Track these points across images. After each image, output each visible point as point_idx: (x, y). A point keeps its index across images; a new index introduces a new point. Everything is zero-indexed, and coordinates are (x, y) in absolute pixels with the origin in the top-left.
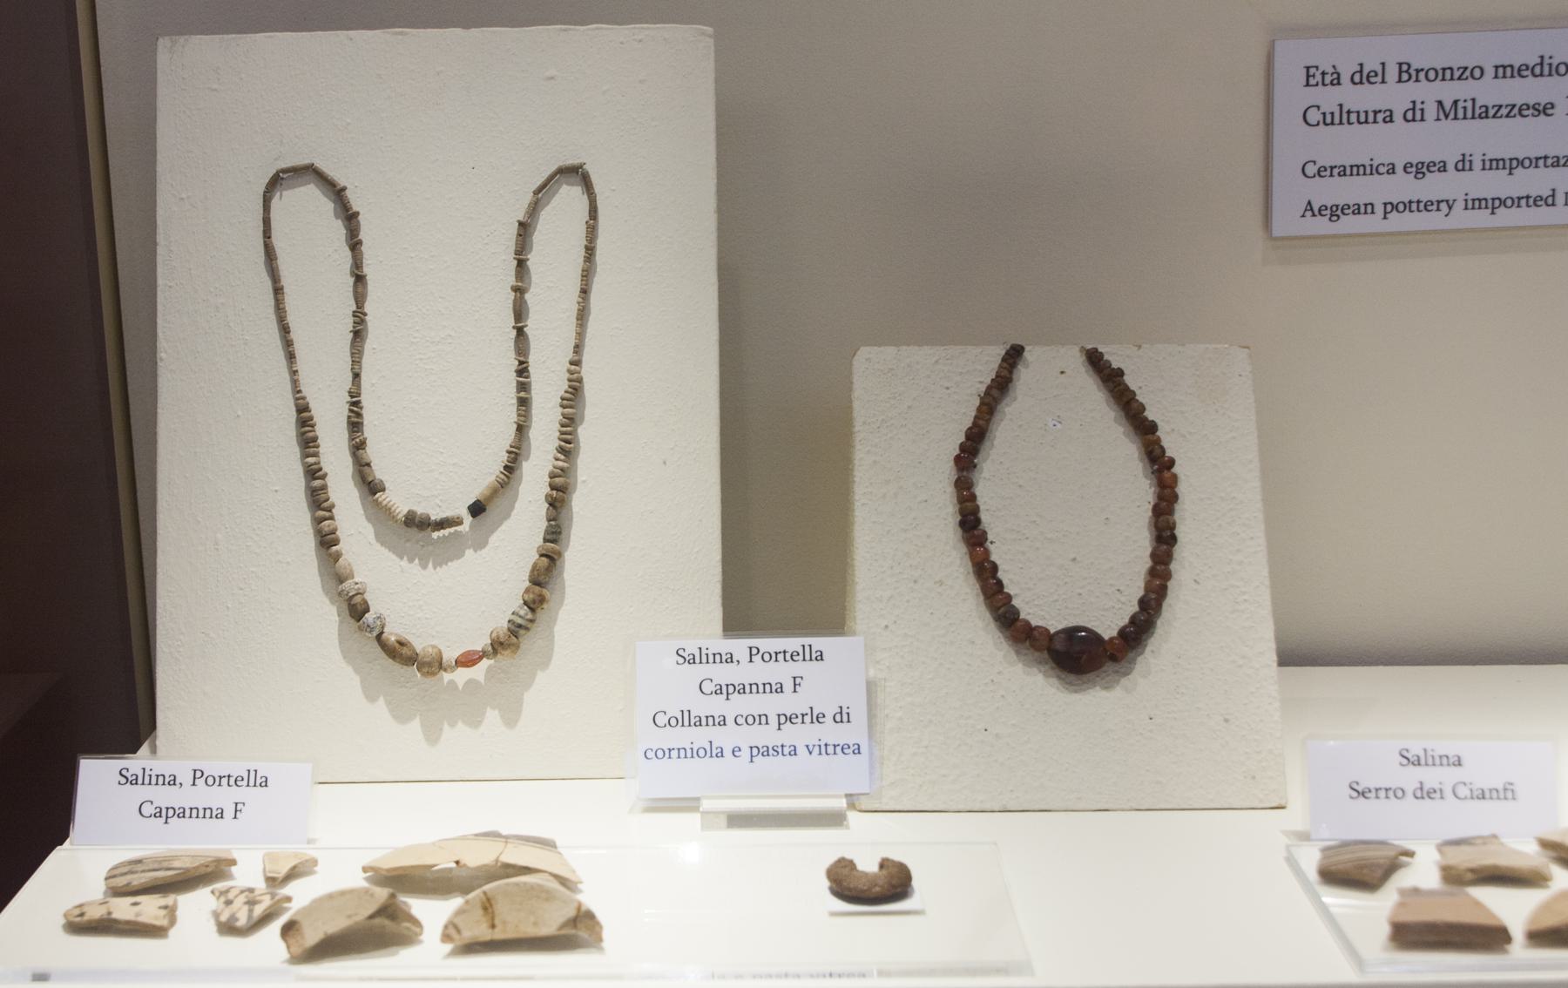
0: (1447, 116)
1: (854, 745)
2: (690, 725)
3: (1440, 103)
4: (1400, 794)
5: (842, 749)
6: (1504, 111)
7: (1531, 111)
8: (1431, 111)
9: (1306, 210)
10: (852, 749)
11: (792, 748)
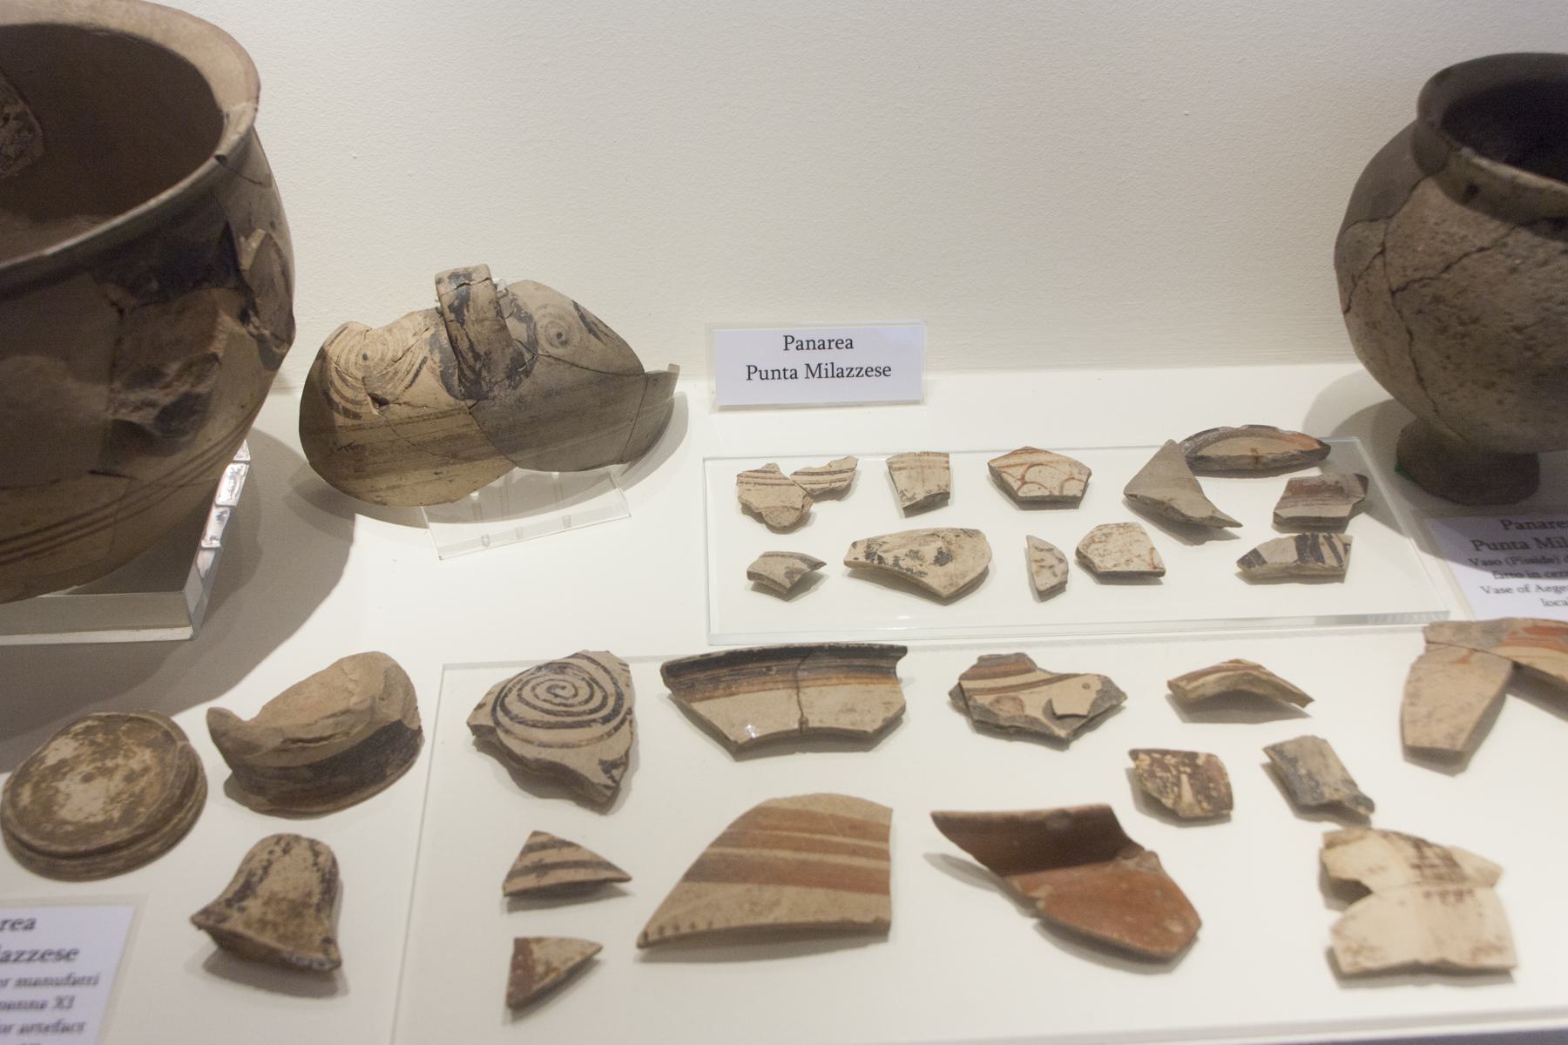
0: (813, 376)
2: (814, 348)
5: (837, 344)
8: (802, 372)
10: (845, 344)
11: (793, 372)
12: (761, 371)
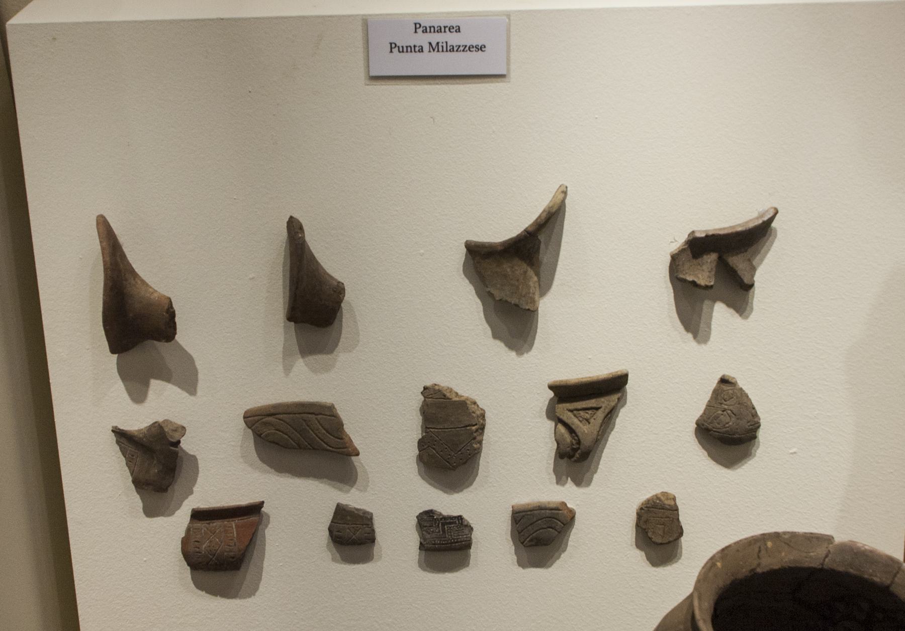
0: (434, 50)
3: (430, 44)
6: (462, 48)
7: (474, 49)
8: (426, 47)
10: (455, 29)
11: (420, 48)
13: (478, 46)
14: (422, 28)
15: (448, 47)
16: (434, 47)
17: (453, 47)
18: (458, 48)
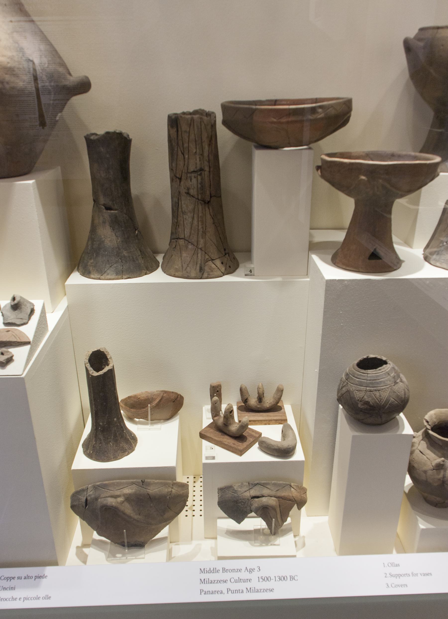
1: (220, 591)
4: (390, 565)
8: (245, 590)
9: (245, 570)
10: (220, 592)
11: (242, 591)
12: (231, 591)
13: (224, 580)
14: (204, 592)
15: (209, 581)
16: (249, 590)
17: (258, 590)
18: (214, 582)
